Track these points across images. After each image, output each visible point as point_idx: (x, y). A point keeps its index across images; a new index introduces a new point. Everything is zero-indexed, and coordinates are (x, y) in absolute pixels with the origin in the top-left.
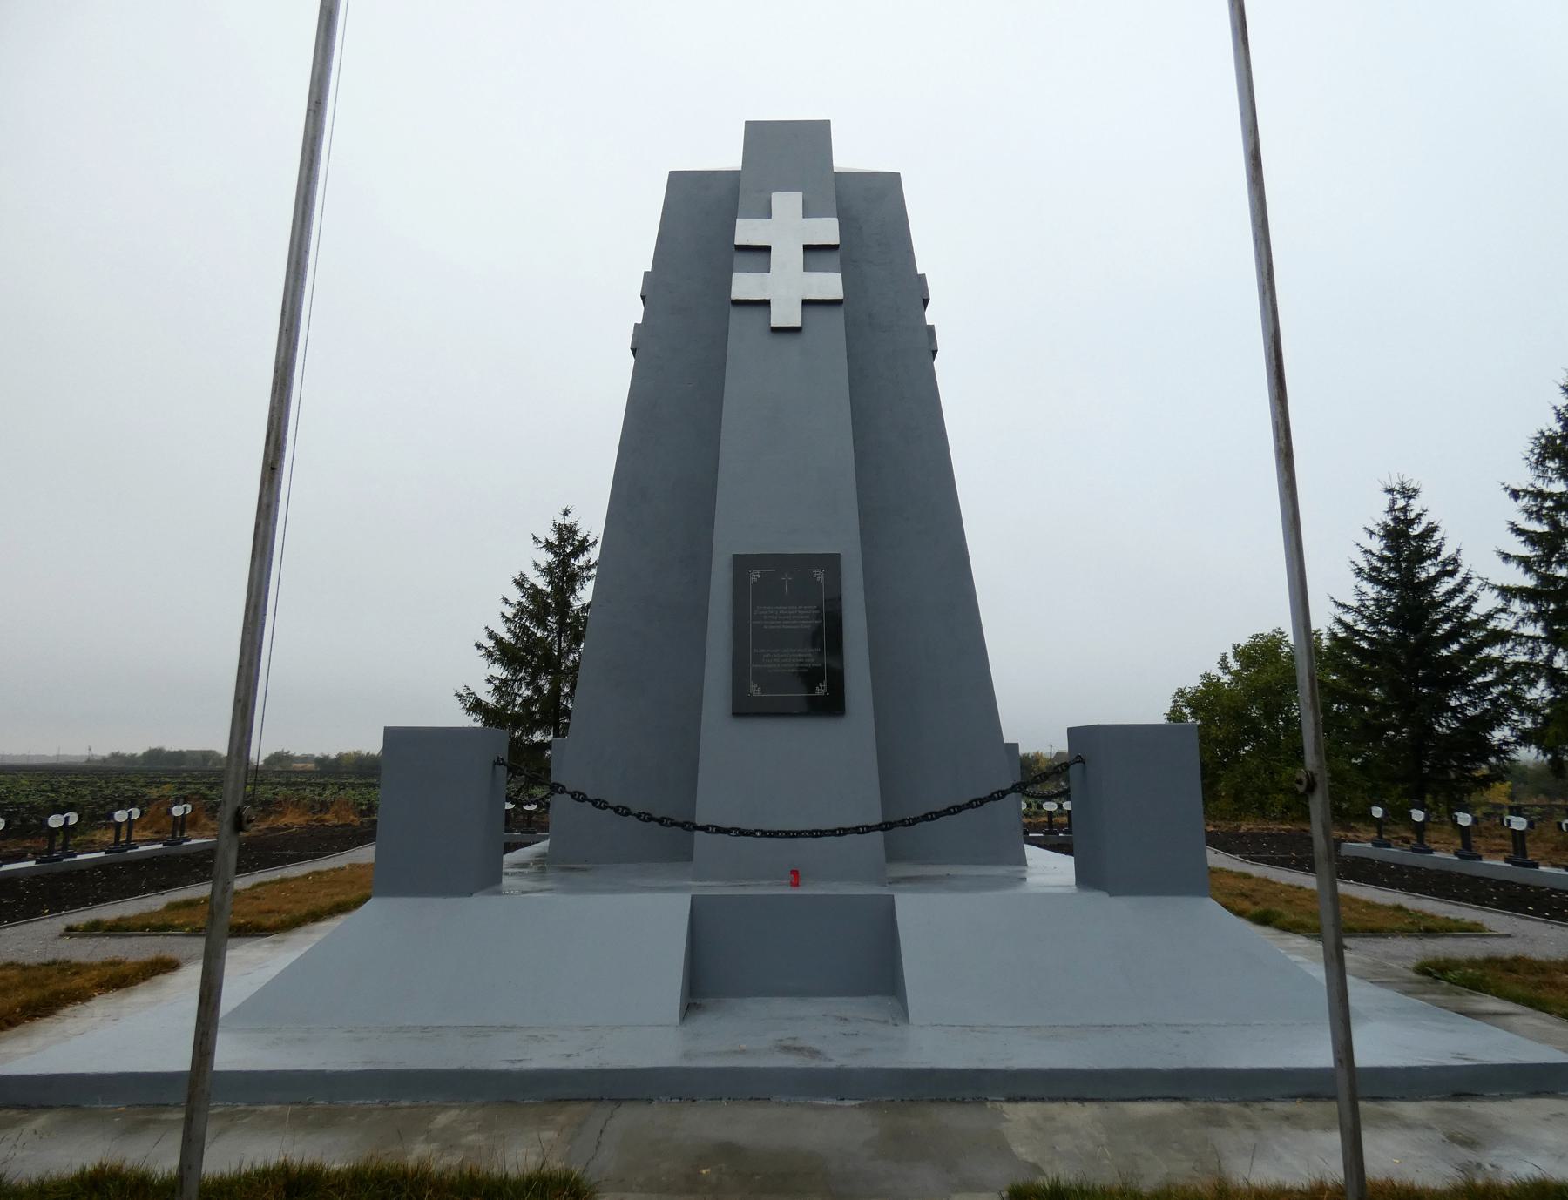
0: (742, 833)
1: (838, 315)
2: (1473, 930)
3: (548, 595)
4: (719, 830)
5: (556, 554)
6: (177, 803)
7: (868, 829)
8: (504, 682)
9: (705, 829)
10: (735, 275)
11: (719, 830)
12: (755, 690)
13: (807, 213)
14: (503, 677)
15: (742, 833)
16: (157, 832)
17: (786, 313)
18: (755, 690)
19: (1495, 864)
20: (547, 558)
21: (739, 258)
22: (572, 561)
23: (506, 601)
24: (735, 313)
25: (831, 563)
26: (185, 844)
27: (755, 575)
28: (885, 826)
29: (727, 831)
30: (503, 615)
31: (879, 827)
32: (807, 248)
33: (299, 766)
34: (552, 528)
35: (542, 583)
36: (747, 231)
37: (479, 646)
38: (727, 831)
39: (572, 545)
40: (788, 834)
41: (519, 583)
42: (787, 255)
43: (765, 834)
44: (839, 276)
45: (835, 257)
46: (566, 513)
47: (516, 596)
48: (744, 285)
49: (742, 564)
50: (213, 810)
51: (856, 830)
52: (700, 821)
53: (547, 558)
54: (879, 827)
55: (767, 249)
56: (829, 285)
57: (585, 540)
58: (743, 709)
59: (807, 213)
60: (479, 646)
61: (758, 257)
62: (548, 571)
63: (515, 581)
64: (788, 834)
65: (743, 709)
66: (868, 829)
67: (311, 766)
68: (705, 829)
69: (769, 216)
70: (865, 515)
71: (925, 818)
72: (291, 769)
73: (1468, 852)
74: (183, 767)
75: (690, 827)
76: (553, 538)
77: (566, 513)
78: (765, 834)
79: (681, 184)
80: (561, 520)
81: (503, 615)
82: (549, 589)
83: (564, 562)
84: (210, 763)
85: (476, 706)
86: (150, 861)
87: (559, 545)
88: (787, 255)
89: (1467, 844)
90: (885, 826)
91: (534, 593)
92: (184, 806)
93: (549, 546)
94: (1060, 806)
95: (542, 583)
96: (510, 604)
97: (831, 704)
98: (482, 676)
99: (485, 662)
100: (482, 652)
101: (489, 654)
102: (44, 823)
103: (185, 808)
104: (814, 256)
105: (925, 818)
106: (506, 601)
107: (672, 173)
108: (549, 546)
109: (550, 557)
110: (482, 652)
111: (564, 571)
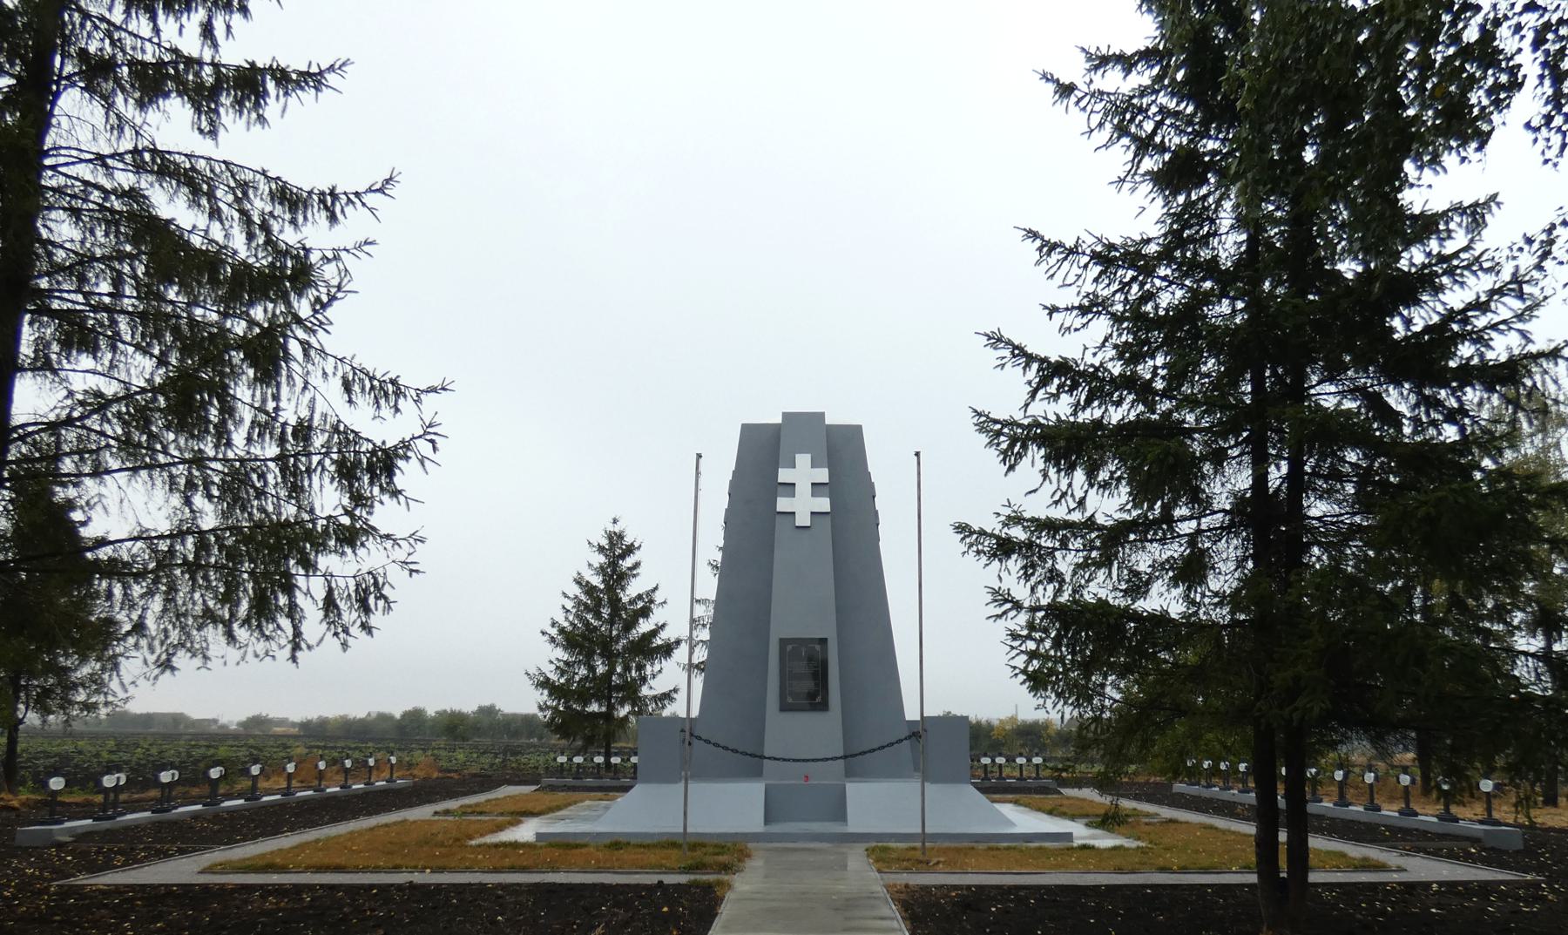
0: (784, 760)
1: (828, 518)
2: (1381, 867)
3: (601, 591)
4: (775, 759)
5: (606, 556)
6: (109, 771)
7: (837, 758)
8: (567, 663)
9: (769, 758)
10: (778, 499)
11: (775, 759)
12: (790, 700)
13: (813, 466)
14: (565, 659)
15: (784, 760)
16: (302, 782)
17: (803, 519)
18: (790, 700)
19: (1390, 811)
20: (601, 559)
21: (780, 489)
22: (621, 562)
23: (565, 595)
24: (778, 516)
25: (823, 641)
26: (174, 811)
27: (789, 648)
28: (845, 757)
29: (778, 759)
30: (564, 607)
31: (841, 758)
32: (812, 513)
33: (278, 730)
34: (603, 533)
35: (596, 581)
36: (784, 475)
37: (543, 633)
38: (778, 759)
39: (621, 548)
40: (804, 760)
41: (578, 582)
42: (803, 489)
43: (794, 760)
44: (827, 470)
45: (827, 488)
46: (615, 521)
47: (575, 590)
48: (783, 504)
49: (783, 642)
50: (451, 756)
51: (832, 759)
52: (766, 755)
53: (601, 559)
54: (841, 758)
55: (794, 484)
56: (824, 504)
57: (632, 544)
58: (785, 707)
59: (813, 466)
60: (543, 633)
61: (789, 488)
62: (601, 570)
63: (575, 580)
64: (804, 760)
65: (785, 707)
66: (837, 758)
67: (295, 731)
68: (769, 758)
69: (794, 467)
70: (840, 610)
71: (860, 754)
72: (270, 733)
73: (1343, 802)
74: (152, 730)
75: (762, 757)
76: (605, 542)
77: (615, 521)
78: (794, 760)
79: (749, 432)
80: (611, 528)
81: (564, 607)
82: (602, 587)
83: (613, 564)
84: (182, 727)
85: (545, 684)
86: (383, 792)
87: (610, 549)
88: (803, 489)
89: (1342, 795)
90: (845, 757)
91: (590, 590)
92: (117, 775)
93: (601, 549)
94: (993, 761)
95: (596, 581)
96: (569, 597)
97: (823, 706)
98: (549, 658)
99: (550, 647)
100: (547, 637)
101: (553, 640)
102: (206, 774)
103: (118, 779)
104: (815, 516)
105: (860, 754)
106: (565, 595)
107: (743, 425)
108: (601, 549)
109: (602, 559)
110: (547, 637)
111: (614, 571)
